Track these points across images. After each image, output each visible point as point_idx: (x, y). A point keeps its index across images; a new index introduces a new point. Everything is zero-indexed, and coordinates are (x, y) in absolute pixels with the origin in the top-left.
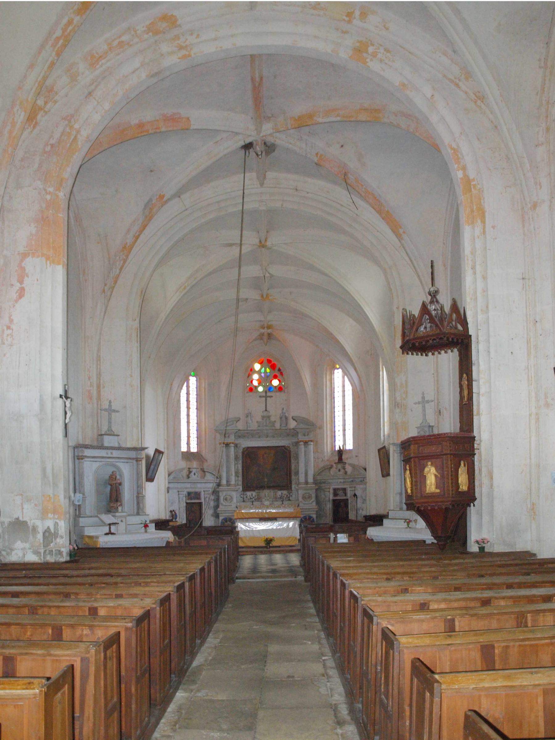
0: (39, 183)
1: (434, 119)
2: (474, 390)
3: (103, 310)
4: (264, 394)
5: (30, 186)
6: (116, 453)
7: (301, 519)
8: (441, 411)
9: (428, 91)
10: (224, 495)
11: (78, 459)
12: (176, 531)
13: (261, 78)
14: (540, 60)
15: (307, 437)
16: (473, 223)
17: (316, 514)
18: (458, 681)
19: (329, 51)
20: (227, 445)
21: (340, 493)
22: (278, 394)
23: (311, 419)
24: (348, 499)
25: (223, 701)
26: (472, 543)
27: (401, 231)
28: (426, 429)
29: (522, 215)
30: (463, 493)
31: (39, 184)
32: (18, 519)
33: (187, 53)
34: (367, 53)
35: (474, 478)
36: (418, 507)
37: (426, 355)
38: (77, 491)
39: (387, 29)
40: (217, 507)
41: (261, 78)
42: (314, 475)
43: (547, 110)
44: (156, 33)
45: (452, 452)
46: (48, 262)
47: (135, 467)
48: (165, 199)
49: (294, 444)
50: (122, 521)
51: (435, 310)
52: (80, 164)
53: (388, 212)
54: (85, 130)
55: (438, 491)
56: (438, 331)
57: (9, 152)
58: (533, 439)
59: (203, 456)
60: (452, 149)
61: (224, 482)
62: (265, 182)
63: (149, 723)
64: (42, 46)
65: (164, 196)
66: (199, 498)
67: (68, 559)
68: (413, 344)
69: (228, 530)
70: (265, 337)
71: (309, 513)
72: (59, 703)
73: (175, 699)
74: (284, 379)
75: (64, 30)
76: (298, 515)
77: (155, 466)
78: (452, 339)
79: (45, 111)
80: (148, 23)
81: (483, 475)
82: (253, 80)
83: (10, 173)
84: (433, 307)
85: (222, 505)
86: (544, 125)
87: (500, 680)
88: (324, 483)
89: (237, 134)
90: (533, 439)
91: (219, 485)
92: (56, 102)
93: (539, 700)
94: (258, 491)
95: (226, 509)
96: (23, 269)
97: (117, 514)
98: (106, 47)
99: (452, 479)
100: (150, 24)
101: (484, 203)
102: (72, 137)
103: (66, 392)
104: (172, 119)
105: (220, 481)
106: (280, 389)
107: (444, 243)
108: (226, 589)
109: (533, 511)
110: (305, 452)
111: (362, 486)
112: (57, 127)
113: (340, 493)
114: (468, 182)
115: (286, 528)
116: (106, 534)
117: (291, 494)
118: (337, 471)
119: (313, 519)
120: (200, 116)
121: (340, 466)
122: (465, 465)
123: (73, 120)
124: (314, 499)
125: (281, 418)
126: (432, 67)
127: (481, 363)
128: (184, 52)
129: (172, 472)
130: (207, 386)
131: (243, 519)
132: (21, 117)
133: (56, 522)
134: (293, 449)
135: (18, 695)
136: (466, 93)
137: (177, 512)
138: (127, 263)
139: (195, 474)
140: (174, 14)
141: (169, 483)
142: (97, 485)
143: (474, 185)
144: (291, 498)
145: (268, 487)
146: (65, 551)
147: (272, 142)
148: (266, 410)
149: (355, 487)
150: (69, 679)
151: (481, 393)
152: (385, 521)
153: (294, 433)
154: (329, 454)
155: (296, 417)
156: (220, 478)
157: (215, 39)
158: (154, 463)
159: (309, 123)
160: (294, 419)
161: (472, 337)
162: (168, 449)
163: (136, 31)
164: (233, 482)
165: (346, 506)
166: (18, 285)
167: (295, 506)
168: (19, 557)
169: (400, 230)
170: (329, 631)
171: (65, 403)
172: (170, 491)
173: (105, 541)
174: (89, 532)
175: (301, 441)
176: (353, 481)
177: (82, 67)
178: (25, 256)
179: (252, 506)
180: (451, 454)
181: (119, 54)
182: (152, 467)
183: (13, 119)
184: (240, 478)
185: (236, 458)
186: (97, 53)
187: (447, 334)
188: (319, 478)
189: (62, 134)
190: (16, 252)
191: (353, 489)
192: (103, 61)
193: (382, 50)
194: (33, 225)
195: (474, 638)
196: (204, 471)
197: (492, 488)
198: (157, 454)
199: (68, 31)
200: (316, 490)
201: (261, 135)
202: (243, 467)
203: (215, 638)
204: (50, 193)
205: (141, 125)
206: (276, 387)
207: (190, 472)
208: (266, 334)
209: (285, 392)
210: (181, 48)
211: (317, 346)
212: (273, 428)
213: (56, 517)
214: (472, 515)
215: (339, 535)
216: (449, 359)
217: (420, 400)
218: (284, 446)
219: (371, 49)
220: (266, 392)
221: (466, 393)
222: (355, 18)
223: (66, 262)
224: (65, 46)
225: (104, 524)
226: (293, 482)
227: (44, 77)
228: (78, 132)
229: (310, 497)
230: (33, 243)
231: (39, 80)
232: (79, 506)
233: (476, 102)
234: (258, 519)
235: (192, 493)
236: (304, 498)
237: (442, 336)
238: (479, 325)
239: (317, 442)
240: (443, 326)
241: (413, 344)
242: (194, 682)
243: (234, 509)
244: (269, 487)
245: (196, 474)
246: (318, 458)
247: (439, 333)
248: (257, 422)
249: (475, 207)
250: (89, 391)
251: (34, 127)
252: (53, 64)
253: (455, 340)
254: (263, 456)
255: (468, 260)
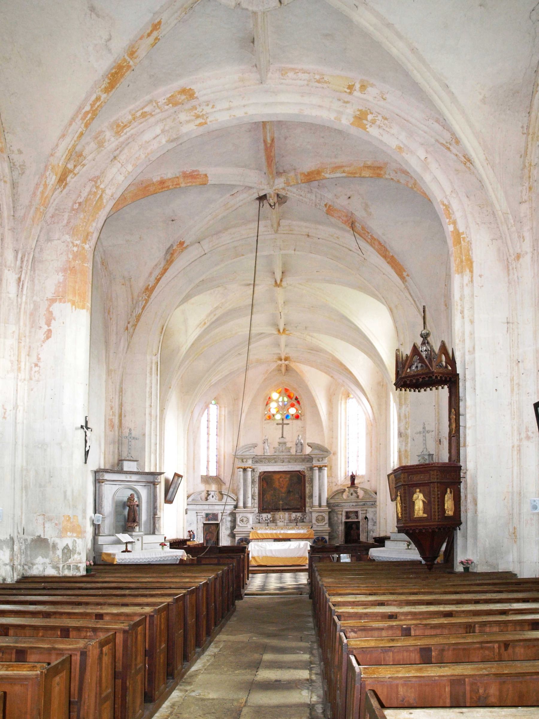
0: (67, 236)
1: (427, 178)
2: (461, 424)
3: (126, 346)
4: (281, 422)
5: (59, 239)
6: (134, 478)
7: (314, 540)
8: (442, 440)
9: (421, 153)
10: (241, 516)
11: (99, 482)
12: (189, 550)
13: (273, 140)
14: (522, 127)
15: (320, 462)
16: (462, 272)
17: (329, 536)
18: (378, 672)
19: (332, 119)
20: (245, 470)
21: (352, 515)
22: (295, 421)
23: (326, 446)
24: (359, 522)
25: (213, 699)
26: (458, 564)
27: (405, 274)
28: (426, 457)
29: (508, 265)
30: (449, 517)
31: (67, 238)
32: (39, 536)
33: (204, 121)
34: (367, 120)
35: (460, 504)
36: (408, 530)
37: (419, 391)
38: (97, 512)
39: (384, 99)
40: (233, 528)
41: (273, 140)
42: (327, 499)
43: (530, 171)
44: (175, 104)
45: (438, 481)
46: (74, 307)
47: (152, 491)
48: (185, 245)
49: (309, 469)
50: (138, 540)
51: (426, 351)
52: (105, 218)
53: (392, 256)
54: (110, 189)
55: (425, 515)
56: (427, 371)
57: (41, 210)
58: (515, 468)
59: (222, 479)
60: (444, 205)
61: (241, 504)
62: (279, 229)
63: (143, 715)
64: (73, 120)
65: (184, 242)
66: (217, 520)
67: (84, 573)
68: (405, 382)
69: (239, 550)
70: (283, 369)
71: (322, 534)
72: (58, 684)
73: (169, 699)
74: (301, 407)
75: (92, 105)
76: (311, 537)
77: (174, 489)
78: (441, 377)
79: (74, 173)
80: (169, 95)
81: (469, 501)
82: (265, 142)
83: (41, 228)
84: (425, 348)
85: (239, 526)
86: (527, 185)
87: (413, 672)
88: (337, 506)
89: (250, 188)
90: (515, 468)
91: (236, 507)
92: (84, 165)
93: (447, 690)
94: (274, 513)
95: (242, 529)
96: (51, 313)
97: (134, 533)
98: (130, 117)
99: (438, 505)
100: (170, 97)
101: (472, 254)
102: (98, 196)
103: (86, 422)
104: (192, 176)
105: (237, 503)
106: (297, 417)
107: (446, 285)
108: (233, 604)
109: (514, 535)
110: (319, 476)
111: (373, 510)
112: (85, 187)
113: (352, 515)
114: (457, 235)
115: (300, 549)
116: (123, 552)
117: (305, 516)
118: (350, 495)
119: (326, 541)
120: (216, 173)
121: (352, 490)
122: (451, 493)
123: (99, 181)
124: (327, 521)
125: (296, 445)
126: (425, 132)
127: (468, 399)
128: (200, 121)
129: (191, 495)
130: (226, 415)
131: (258, 539)
132: (53, 179)
133: (74, 540)
134: (307, 474)
135: (24, 675)
136: (456, 155)
137: (195, 533)
138: (149, 304)
139: (213, 497)
140: (192, 88)
141: (188, 504)
142: (116, 506)
143: (464, 238)
144: (305, 520)
145: (283, 509)
146: (83, 566)
147: (284, 194)
148: (282, 437)
149: (366, 510)
150: (68, 666)
151: (468, 426)
152: (387, 543)
153: (309, 459)
154: (343, 479)
155: (311, 443)
156: (237, 500)
157: (229, 109)
158: (173, 486)
159: (318, 178)
160: (309, 446)
161: (460, 375)
162: (187, 472)
163: (157, 103)
164: (249, 504)
165: (358, 528)
166: (45, 328)
167: (309, 528)
168: (40, 571)
169: (404, 273)
170: (321, 645)
171: (86, 432)
172: (188, 512)
173: (120, 557)
174: (108, 550)
175: (315, 466)
176: (364, 505)
177: (108, 134)
178: (52, 301)
179: (267, 527)
180: (438, 482)
181: (141, 123)
182: (171, 490)
183: (45, 182)
184: (256, 501)
185: (253, 482)
186: (122, 123)
187: (436, 373)
188: (332, 501)
189: (90, 193)
190: (45, 298)
191: (365, 512)
192: (128, 129)
193: (380, 118)
194: (61, 274)
195: (414, 642)
196: (222, 494)
197: (476, 513)
198: (176, 478)
199: (96, 106)
200: (330, 512)
201: (274, 188)
202: (259, 490)
203: (216, 647)
204: (77, 245)
205: (162, 182)
206: (293, 415)
207: (209, 495)
208: (283, 365)
209: (301, 420)
210: (198, 117)
211: (332, 377)
212: (289, 454)
213: (75, 535)
214: (458, 537)
215: (342, 555)
216: (444, 392)
217: (422, 430)
218: (299, 471)
219: (370, 117)
220: (283, 420)
221: (454, 426)
222: (355, 90)
223: (90, 307)
224: (92, 119)
225: (119, 542)
226: (307, 505)
227: (73, 145)
228: (103, 191)
229: (323, 519)
230: (61, 290)
231: (69, 148)
232: (99, 525)
233: (465, 164)
234: (273, 540)
235: (210, 514)
236: (317, 520)
237: (431, 375)
238: (466, 364)
239: (331, 467)
240: (432, 366)
241: (405, 382)
242: (190, 683)
243: (249, 530)
244: (284, 510)
245: (214, 497)
246: (332, 483)
247: (427, 371)
248: (274, 448)
249: (464, 258)
250: (111, 420)
251: (64, 187)
252: (82, 134)
253: (444, 379)
254: (279, 479)
255: (457, 305)
